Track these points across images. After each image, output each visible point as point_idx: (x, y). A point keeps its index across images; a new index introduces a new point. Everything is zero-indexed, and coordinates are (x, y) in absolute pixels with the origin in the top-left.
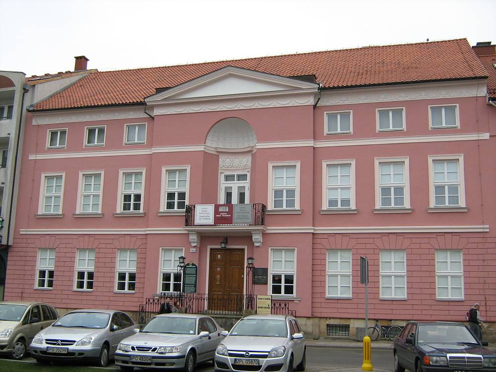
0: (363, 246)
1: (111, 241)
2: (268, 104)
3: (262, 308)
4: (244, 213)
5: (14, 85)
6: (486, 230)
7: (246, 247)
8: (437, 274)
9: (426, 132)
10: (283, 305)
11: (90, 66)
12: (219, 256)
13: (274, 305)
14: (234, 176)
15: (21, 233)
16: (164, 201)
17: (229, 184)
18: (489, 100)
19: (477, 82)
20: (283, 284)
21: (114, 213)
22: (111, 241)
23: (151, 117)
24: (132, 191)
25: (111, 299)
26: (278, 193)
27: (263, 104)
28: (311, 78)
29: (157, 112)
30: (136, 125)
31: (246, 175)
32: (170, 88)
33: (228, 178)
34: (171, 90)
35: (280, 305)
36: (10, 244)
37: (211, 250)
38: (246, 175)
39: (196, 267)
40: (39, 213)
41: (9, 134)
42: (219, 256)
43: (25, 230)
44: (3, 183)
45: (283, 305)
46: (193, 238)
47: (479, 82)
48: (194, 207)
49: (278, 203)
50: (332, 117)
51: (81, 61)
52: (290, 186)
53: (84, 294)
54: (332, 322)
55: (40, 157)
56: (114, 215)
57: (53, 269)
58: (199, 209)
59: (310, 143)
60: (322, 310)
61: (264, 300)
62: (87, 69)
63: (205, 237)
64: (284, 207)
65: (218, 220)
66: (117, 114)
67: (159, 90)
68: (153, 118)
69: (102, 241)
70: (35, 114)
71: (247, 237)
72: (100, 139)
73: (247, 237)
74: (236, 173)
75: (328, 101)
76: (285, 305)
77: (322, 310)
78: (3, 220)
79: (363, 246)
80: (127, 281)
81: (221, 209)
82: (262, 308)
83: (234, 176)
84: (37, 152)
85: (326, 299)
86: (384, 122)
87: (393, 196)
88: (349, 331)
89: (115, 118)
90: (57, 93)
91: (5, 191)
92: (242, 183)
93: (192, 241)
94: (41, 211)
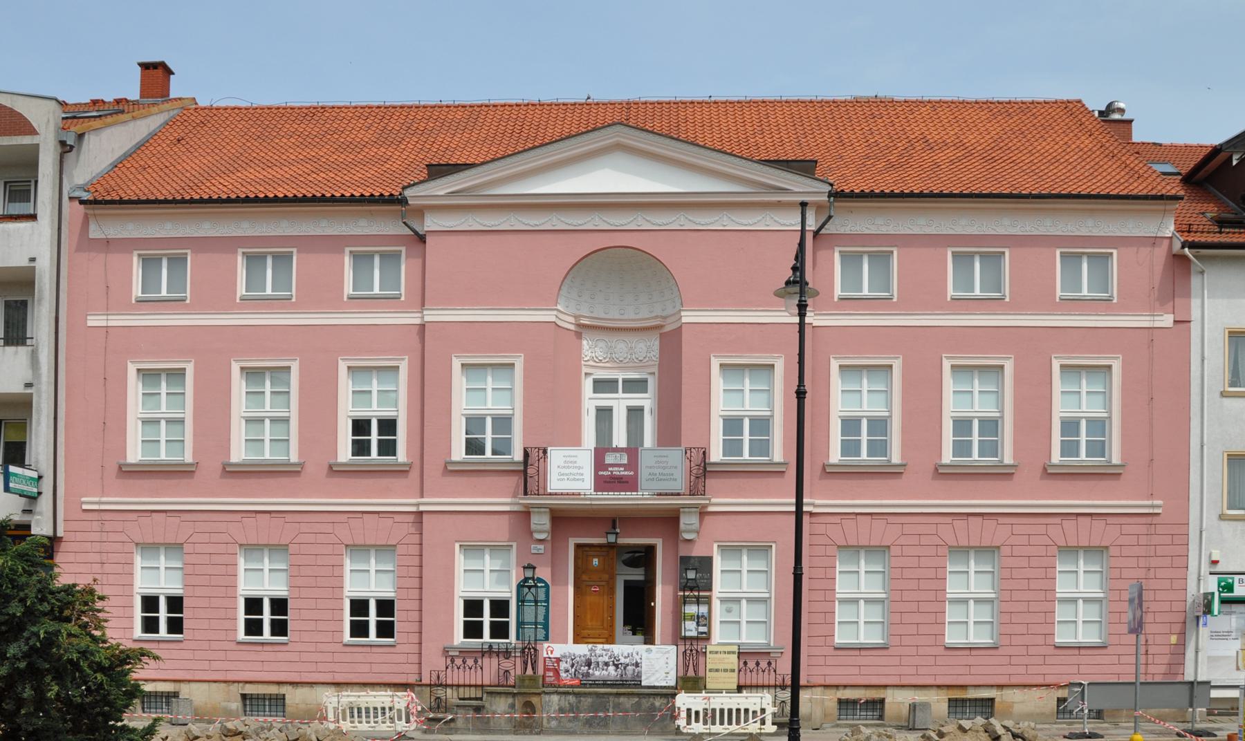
0: (915, 540)
1: (329, 528)
2: (708, 220)
3: (717, 670)
4: (664, 468)
5: (32, 131)
6: (1156, 511)
7: (658, 543)
8: (1058, 595)
9: (939, 304)
10: (764, 664)
11: (177, 88)
12: (596, 561)
13: (745, 663)
14: (616, 381)
15: (84, 507)
16: (345, 437)
17: (605, 400)
18: (1183, 247)
19: (1162, 207)
20: (487, 619)
21: (122, 462)
22: (329, 528)
23: (416, 233)
24: (375, 411)
25: (337, 657)
26: (733, 425)
27: (612, 221)
28: (805, 167)
29: (431, 223)
30: (1083, 253)
31: (645, 381)
32: (472, 166)
33: (602, 386)
34: (473, 171)
35: (758, 664)
36: (59, 535)
37: (578, 547)
38: (645, 381)
39: (547, 586)
40: (234, 459)
41: (33, 260)
42: (596, 561)
43: (96, 499)
44: (29, 385)
45: (764, 664)
46: (541, 523)
47: (1168, 207)
48: (545, 452)
49: (732, 447)
50: (852, 261)
51: (156, 74)
52: (503, 409)
53: (267, 648)
54: (250, 689)
55: (116, 321)
56: (447, 464)
57: (285, 593)
58: (557, 457)
59: (431, 316)
60: (827, 671)
61: (723, 656)
62: (172, 96)
63: (566, 519)
64: (746, 456)
65: (604, 482)
66: (324, 223)
67: (437, 171)
68: (421, 239)
69: (304, 528)
70: (99, 210)
71: (668, 521)
72: (282, 280)
73: (668, 521)
74: (620, 376)
75: (850, 223)
76: (769, 664)
77: (827, 671)
78: (40, 477)
79: (915, 540)
80: (267, 617)
81: (610, 459)
82: (717, 670)
83: (616, 381)
84: (107, 310)
85: (836, 649)
86: (1073, 280)
87: (746, 437)
88: (882, 709)
89: (319, 232)
90: (128, 156)
91: (39, 403)
92: (636, 399)
93: (539, 527)
94: (135, 454)
